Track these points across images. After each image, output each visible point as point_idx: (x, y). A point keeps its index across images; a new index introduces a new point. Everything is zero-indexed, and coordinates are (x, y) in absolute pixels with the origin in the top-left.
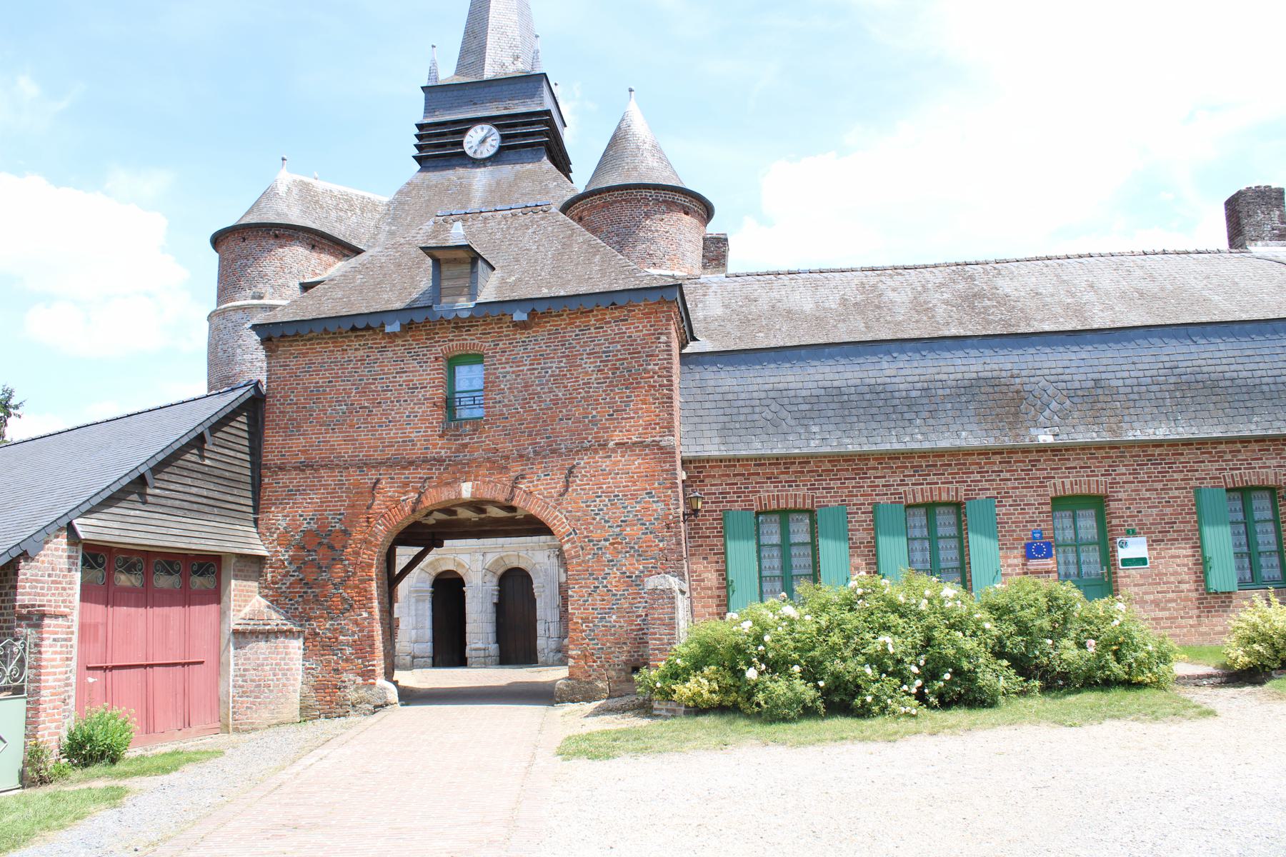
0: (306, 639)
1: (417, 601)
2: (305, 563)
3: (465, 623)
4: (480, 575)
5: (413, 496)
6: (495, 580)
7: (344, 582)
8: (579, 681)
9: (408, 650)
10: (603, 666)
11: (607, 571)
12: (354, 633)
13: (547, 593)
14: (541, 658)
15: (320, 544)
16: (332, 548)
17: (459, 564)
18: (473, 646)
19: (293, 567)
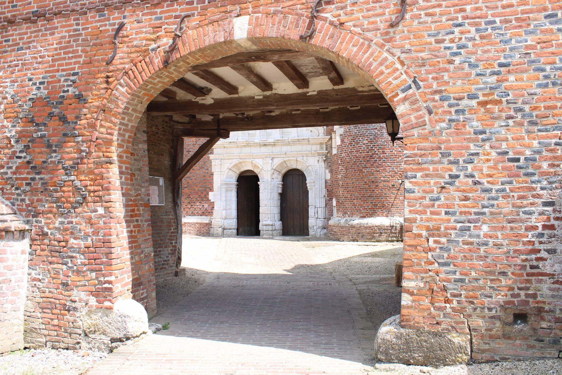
0: (33, 240)
1: (227, 191)
2: (32, 141)
3: (259, 206)
4: (269, 173)
5: (167, 41)
6: (280, 178)
7: (75, 166)
8: (419, 331)
9: (220, 224)
10: (461, 310)
11: (473, 149)
12: (87, 235)
13: (317, 186)
14: (311, 232)
15: (51, 115)
16: (63, 119)
17: (255, 166)
18: (264, 223)
19: (20, 147)
